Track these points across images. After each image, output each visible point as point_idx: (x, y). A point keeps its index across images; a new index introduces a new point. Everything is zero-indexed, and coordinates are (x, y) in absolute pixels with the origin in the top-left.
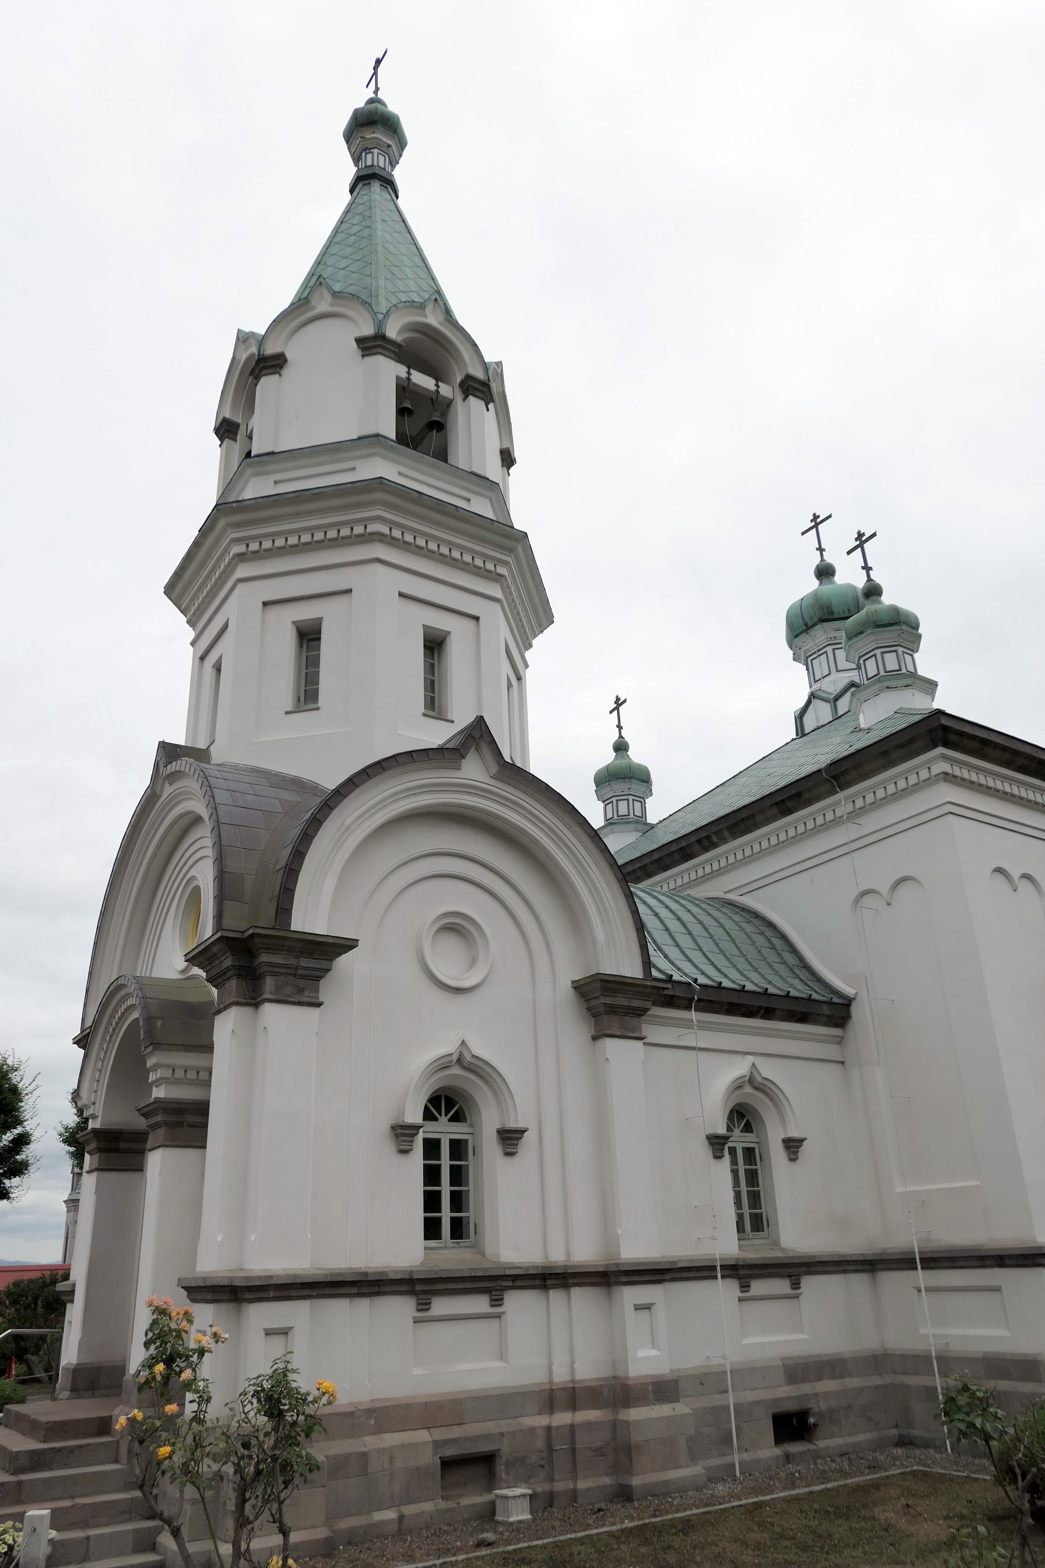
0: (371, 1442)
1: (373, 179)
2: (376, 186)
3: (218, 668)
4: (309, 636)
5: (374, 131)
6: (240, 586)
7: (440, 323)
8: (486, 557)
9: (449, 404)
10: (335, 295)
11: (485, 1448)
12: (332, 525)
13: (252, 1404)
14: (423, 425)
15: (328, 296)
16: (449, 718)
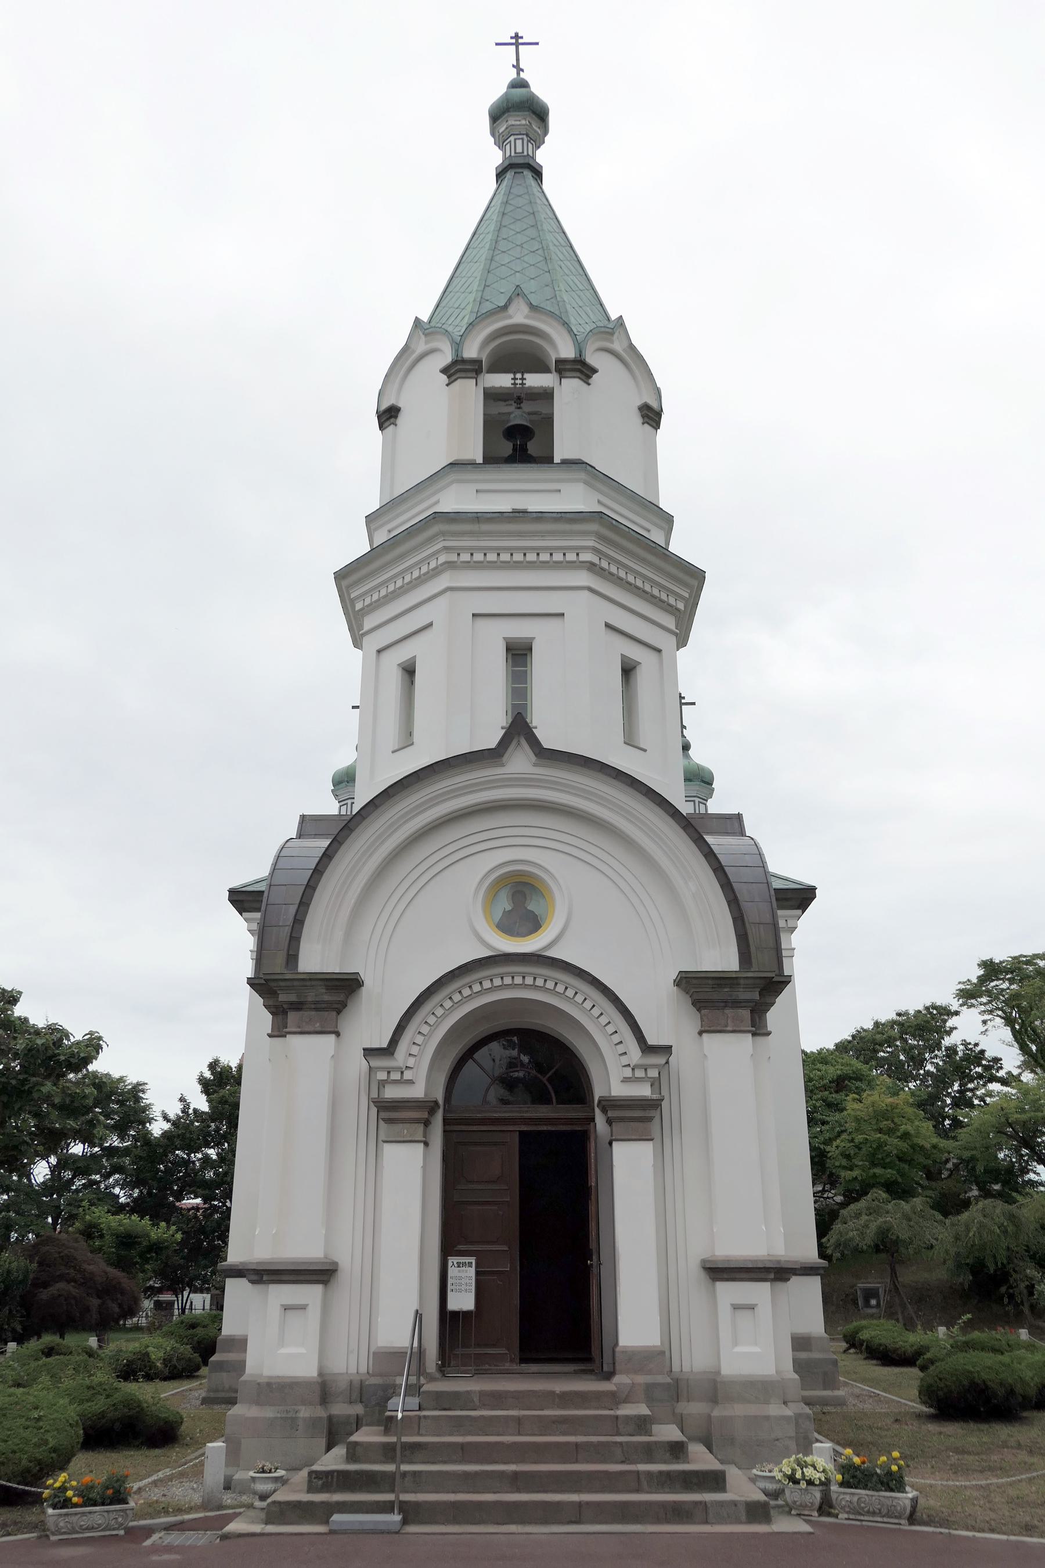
0: (168, 1472)
1: (520, 170)
2: (528, 174)
3: (409, 671)
4: (519, 653)
5: (520, 115)
6: (448, 593)
7: (526, 317)
8: (645, 578)
9: (546, 396)
10: (533, 308)
11: (953, 1431)
12: (518, 549)
13: (37, 1446)
14: (519, 437)
15: (525, 309)
16: (642, 746)
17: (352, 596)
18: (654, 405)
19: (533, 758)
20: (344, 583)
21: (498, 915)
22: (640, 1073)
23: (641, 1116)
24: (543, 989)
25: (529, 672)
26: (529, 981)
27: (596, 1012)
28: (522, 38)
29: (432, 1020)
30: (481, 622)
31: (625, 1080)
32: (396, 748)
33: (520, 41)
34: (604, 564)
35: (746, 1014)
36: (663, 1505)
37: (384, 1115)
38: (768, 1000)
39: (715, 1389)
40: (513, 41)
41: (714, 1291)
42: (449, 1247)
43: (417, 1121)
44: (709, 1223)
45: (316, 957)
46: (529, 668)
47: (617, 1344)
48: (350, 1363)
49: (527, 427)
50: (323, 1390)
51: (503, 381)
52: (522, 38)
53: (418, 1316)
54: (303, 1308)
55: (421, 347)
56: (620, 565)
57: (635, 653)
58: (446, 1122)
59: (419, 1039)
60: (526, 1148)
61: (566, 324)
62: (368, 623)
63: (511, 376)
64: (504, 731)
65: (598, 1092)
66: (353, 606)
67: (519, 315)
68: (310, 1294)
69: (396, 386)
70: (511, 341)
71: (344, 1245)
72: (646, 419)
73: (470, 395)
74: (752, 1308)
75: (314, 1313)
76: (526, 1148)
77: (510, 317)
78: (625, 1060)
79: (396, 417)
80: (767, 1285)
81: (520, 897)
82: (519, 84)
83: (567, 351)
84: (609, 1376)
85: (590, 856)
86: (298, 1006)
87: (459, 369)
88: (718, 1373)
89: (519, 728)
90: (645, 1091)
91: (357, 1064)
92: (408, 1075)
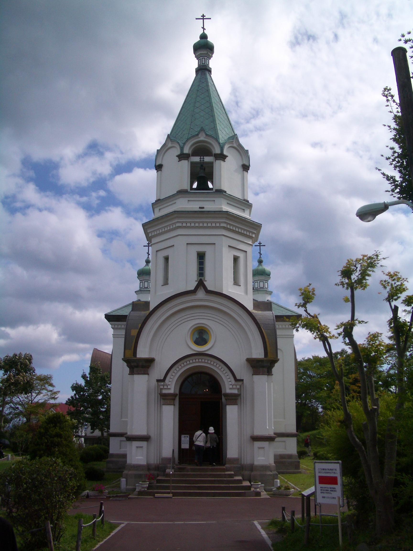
1: (203, 71)
3: (167, 259)
4: (201, 257)
14: (202, 176)
15: (204, 135)
17: (148, 232)
18: (247, 164)
19: (205, 293)
20: (146, 227)
22: (234, 387)
23: (234, 399)
24: (207, 363)
26: (203, 361)
27: (222, 370)
29: (175, 371)
30: (189, 246)
31: (230, 389)
33: (204, 17)
34: (228, 227)
35: (266, 370)
36: (162, 483)
39: (252, 468)
40: (202, 17)
41: (253, 445)
43: (172, 399)
44: (262, 417)
45: (142, 352)
48: (154, 461)
49: (204, 177)
50: (148, 467)
51: (197, 159)
53: (173, 450)
54: (142, 447)
55: (170, 145)
56: (233, 226)
57: (237, 254)
59: (172, 377)
60: (202, 399)
62: (154, 241)
63: (199, 157)
64: (197, 282)
67: (202, 137)
68: (144, 444)
69: (161, 157)
71: (147, 425)
73: (185, 165)
74: (263, 448)
75: (145, 449)
76: (202, 399)
77: (199, 138)
78: (230, 383)
80: (268, 442)
81: (201, 336)
82: (204, 37)
84: (224, 465)
86: (137, 366)
87: (182, 157)
88: (253, 464)
89: (201, 284)
90: (236, 392)
91: (154, 383)
92: (169, 387)
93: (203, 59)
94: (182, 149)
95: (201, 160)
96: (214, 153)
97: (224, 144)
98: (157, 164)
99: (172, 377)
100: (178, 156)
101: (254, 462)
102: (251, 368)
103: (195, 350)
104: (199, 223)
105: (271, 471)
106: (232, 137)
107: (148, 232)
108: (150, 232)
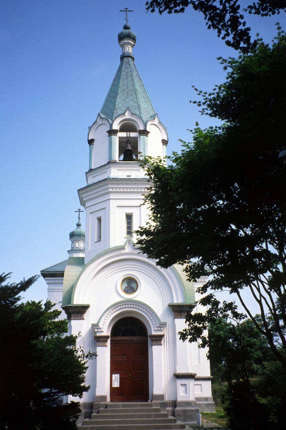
9: (136, 140)
17: (83, 196)
20: (80, 193)
21: (124, 288)
25: (131, 222)
28: (80, 210)
31: (155, 330)
32: (98, 241)
37: (96, 340)
38: (191, 310)
40: (125, 10)
42: (112, 372)
46: (131, 225)
47: (153, 394)
51: (124, 134)
52: (80, 210)
58: (111, 341)
59: (108, 316)
61: (140, 117)
62: (87, 204)
65: (149, 334)
66: (83, 200)
67: (127, 115)
70: (125, 123)
72: (164, 144)
79: (93, 142)
83: (142, 128)
85: (147, 273)
88: (177, 400)
93: (127, 48)
94: (111, 125)
95: (127, 136)
96: (138, 129)
97: (147, 122)
98: (90, 139)
99: (108, 316)
100: (108, 132)
101: (177, 399)
102: (173, 312)
103: (125, 298)
104: (123, 188)
105: (193, 407)
106: (153, 115)
107: (83, 196)
108: (84, 197)
